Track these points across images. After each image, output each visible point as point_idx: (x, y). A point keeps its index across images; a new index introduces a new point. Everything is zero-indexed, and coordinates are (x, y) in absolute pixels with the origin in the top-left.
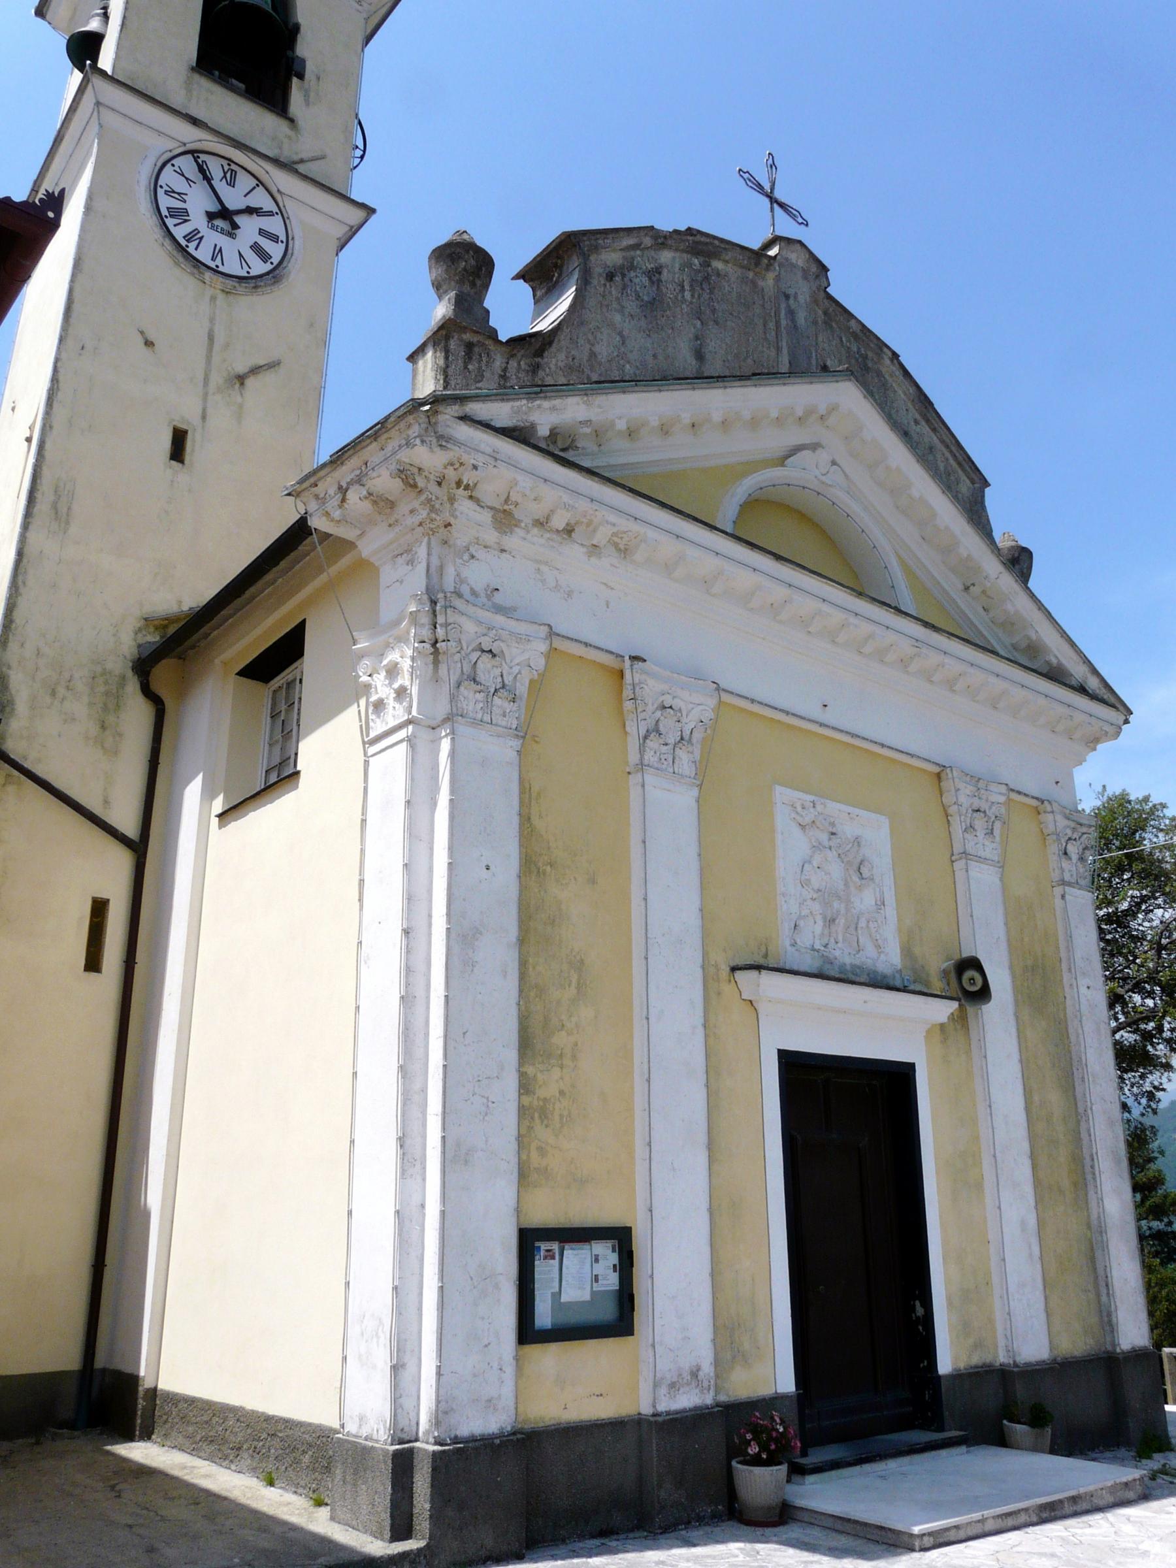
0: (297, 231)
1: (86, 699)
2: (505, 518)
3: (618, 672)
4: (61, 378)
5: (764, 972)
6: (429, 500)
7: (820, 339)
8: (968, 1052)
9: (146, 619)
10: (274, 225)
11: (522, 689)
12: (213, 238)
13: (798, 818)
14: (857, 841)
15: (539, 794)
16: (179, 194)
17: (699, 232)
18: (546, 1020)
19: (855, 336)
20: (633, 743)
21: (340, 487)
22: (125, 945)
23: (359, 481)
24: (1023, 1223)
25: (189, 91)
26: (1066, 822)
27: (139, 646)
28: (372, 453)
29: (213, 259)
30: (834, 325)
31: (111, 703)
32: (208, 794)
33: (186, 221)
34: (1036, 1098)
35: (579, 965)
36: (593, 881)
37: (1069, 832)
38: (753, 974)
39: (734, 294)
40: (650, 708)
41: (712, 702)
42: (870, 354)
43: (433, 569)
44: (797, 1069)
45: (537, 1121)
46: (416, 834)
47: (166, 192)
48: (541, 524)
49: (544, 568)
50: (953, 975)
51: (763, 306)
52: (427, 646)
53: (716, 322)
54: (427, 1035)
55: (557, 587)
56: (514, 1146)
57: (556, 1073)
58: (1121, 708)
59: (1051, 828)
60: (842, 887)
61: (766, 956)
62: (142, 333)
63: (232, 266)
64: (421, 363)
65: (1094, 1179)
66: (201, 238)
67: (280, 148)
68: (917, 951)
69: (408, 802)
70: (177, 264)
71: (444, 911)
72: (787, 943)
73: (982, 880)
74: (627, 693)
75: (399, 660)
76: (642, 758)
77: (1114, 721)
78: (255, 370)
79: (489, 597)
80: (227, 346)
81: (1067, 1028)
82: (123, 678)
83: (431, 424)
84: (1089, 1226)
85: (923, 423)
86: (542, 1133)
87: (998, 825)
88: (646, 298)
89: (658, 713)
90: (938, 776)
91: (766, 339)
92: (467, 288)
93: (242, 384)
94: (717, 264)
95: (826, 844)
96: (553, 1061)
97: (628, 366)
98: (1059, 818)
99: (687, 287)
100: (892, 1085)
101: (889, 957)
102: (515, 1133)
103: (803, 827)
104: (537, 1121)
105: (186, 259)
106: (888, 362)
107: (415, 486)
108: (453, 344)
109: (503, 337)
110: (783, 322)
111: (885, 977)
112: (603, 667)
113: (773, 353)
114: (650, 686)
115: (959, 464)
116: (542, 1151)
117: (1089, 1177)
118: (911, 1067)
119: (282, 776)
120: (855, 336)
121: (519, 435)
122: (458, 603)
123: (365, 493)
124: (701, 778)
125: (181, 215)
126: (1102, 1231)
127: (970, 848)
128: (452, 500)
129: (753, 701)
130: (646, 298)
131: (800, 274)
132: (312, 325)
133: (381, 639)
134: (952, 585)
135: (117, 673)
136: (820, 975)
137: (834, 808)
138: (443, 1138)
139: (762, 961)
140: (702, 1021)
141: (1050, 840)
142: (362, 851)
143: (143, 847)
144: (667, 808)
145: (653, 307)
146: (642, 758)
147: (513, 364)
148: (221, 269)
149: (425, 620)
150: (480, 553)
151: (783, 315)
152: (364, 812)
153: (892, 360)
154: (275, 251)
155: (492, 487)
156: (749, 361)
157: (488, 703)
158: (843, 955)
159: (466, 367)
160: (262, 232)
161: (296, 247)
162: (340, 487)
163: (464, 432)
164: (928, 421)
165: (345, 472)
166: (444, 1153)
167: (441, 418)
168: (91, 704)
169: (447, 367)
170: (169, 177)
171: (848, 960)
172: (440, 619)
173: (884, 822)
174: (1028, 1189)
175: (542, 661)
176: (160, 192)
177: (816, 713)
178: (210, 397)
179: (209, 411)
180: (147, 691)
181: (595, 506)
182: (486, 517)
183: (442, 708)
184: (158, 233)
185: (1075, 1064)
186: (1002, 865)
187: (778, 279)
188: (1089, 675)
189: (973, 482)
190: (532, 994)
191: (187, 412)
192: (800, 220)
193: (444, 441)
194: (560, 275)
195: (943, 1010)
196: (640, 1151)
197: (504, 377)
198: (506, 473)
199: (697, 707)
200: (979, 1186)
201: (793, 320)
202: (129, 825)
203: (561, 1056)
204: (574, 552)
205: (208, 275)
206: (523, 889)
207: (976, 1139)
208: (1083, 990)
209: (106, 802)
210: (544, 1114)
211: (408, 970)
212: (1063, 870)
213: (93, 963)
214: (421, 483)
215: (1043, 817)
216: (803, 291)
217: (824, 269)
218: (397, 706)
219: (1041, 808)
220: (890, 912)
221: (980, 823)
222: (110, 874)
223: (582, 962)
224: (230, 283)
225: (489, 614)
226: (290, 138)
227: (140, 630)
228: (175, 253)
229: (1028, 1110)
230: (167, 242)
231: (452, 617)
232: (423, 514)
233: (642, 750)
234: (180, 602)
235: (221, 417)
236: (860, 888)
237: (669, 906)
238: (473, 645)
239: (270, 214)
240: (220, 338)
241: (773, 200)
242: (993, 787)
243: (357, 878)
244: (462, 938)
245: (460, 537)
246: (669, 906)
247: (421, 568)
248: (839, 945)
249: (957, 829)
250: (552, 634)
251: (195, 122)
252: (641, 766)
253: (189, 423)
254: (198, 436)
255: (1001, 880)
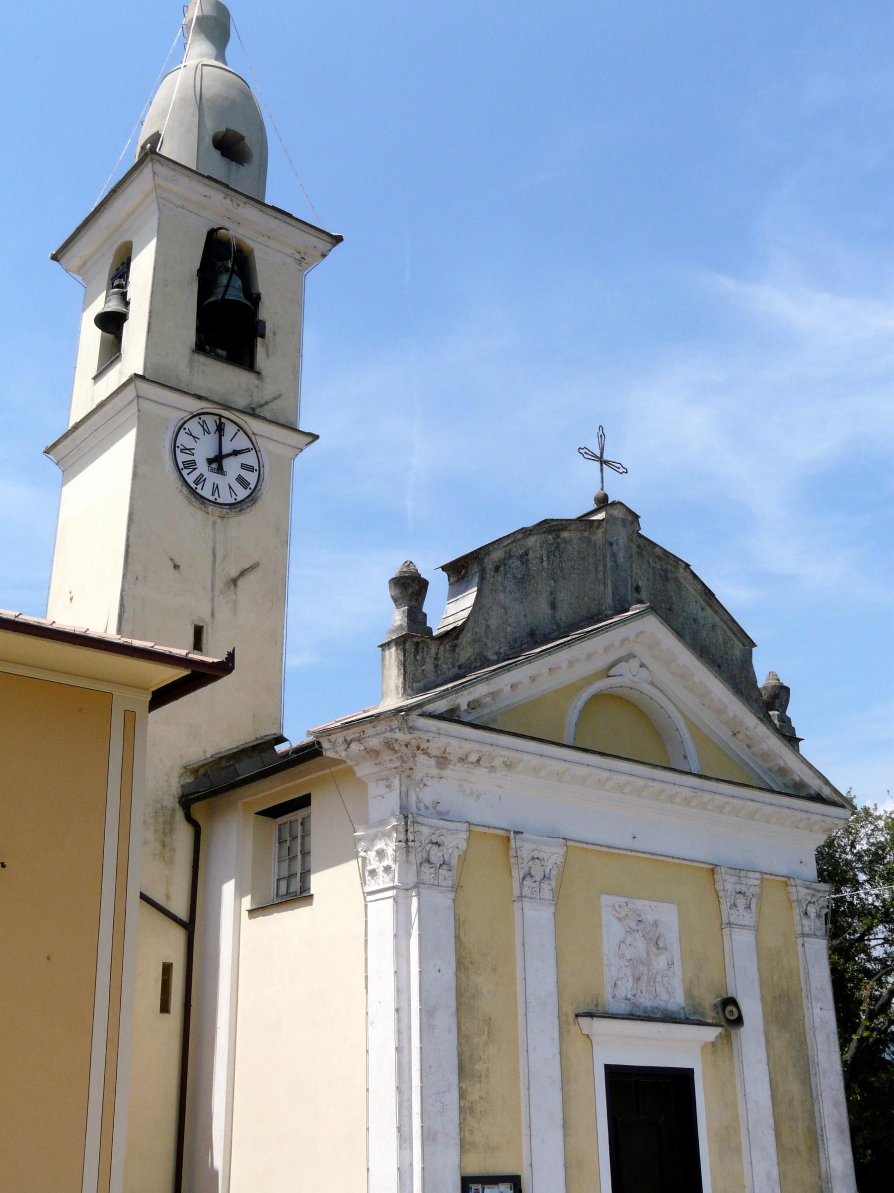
0: (266, 460)
1: (152, 828)
2: (443, 760)
3: (507, 838)
4: (125, 603)
5: (595, 1019)
6: (401, 757)
7: (634, 566)
8: (731, 1059)
9: (185, 767)
10: (250, 459)
11: (454, 862)
12: (212, 478)
13: (617, 915)
14: (656, 924)
15: (464, 922)
16: (189, 450)
17: (552, 520)
18: (472, 1055)
19: (659, 558)
20: (516, 884)
21: (346, 740)
22: (187, 995)
23: (359, 740)
24: (768, 1175)
25: (191, 368)
26: (807, 891)
27: (182, 786)
28: (369, 730)
29: (213, 495)
30: (644, 553)
31: (167, 830)
32: (240, 893)
33: (195, 469)
34: (781, 1088)
35: (488, 1021)
36: (494, 970)
37: (809, 898)
38: (589, 1019)
39: (576, 553)
40: (526, 860)
41: (562, 851)
42: (669, 567)
43: (403, 793)
44: (617, 1076)
45: (468, 1114)
46: (401, 954)
47: (182, 451)
48: (462, 760)
49: (464, 783)
50: (720, 1009)
51: (595, 555)
52: (403, 844)
53: (564, 578)
54: (410, 1068)
55: (472, 793)
56: (458, 1130)
57: (477, 1086)
58: (848, 806)
59: (794, 898)
60: (645, 956)
61: (597, 1005)
62: (172, 560)
63: (225, 497)
64: (387, 652)
65: (823, 1144)
66: (205, 480)
67: (252, 396)
68: (696, 993)
69: (395, 935)
70: (190, 503)
71: (418, 998)
72: (610, 997)
73: (742, 944)
74: (512, 853)
75: (385, 847)
76: (521, 893)
77: (844, 816)
78: (243, 573)
79: (434, 808)
80: (224, 559)
81: (805, 1037)
82: (173, 810)
83: (405, 719)
84: (820, 1177)
85: (708, 608)
86: (471, 1122)
87: (754, 901)
88: (519, 576)
89: (531, 863)
90: (713, 870)
91: (597, 579)
92: (414, 603)
93: (235, 585)
94: (565, 535)
95: (635, 928)
96: (476, 1079)
97: (509, 628)
98: (800, 889)
99: (545, 559)
100: (682, 1079)
101: (677, 1000)
102: (458, 1122)
103: (620, 919)
104: (468, 1114)
105: (196, 498)
106: (682, 570)
107: (394, 749)
108: (408, 646)
109: (435, 633)
110: (609, 565)
111: (673, 1012)
112: (497, 836)
113: (602, 587)
114: (525, 847)
115: (734, 633)
116: (471, 1132)
117: (820, 1142)
118: (691, 1071)
119: (295, 894)
120: (659, 558)
121: (451, 716)
122: (420, 819)
123: (362, 748)
124: (557, 900)
125: (191, 465)
126: (828, 1180)
127: (732, 920)
128: (414, 756)
129: (587, 843)
130: (519, 576)
131: (620, 523)
132: (278, 530)
133: (373, 831)
134: (725, 734)
135: (169, 807)
136: (631, 1016)
137: (639, 904)
138: (422, 1127)
139: (593, 1009)
140: (559, 1050)
141: (795, 904)
142: (366, 959)
143: (192, 925)
144: (537, 919)
145: (523, 581)
146: (521, 893)
147: (442, 648)
148: (219, 501)
149: (402, 829)
150: (429, 782)
151: (608, 559)
152: (366, 935)
153: (685, 569)
154: (251, 478)
155: (435, 747)
156: (586, 599)
157: (437, 874)
158: (646, 1001)
159: (415, 659)
160: (244, 466)
161: (266, 473)
162: (346, 740)
163: (423, 722)
164: (711, 606)
165: (350, 734)
166: (422, 1135)
167: (410, 717)
168: (156, 831)
169: (405, 661)
170: (184, 440)
171: (649, 1004)
172: (410, 829)
173: (674, 909)
174: (773, 1151)
175: (465, 844)
176: (178, 451)
177: (628, 843)
178: (216, 599)
179: (216, 610)
180: (189, 819)
181: (494, 748)
182: (433, 762)
183: (412, 879)
184: (178, 483)
185: (811, 1062)
186: (756, 928)
187: (605, 533)
188: (823, 786)
189: (744, 645)
190: (464, 1041)
191: (202, 613)
192: (622, 470)
193: (411, 729)
194: (466, 573)
195: (711, 1034)
196: (525, 1131)
197: (437, 659)
198: (444, 740)
199: (553, 854)
200: (738, 1150)
201: (615, 561)
202: (182, 912)
203: (480, 1076)
204: (481, 772)
205: (210, 508)
206: (458, 979)
207: (736, 1117)
208: (817, 1011)
209: (168, 897)
210: (472, 1111)
211: (399, 1032)
212: (803, 926)
213: (165, 1008)
214: (397, 747)
215: (789, 888)
216: (621, 536)
217: (637, 517)
218: (385, 875)
219: (788, 882)
220: (677, 968)
221: (741, 902)
222: (170, 945)
223: (490, 1019)
224: (225, 510)
225: (435, 821)
226: (257, 386)
227: (182, 775)
228: (189, 495)
229: (773, 1097)
230: (184, 490)
231: (417, 828)
232: (398, 764)
233: (521, 887)
234: (205, 752)
235: (224, 613)
236: (657, 955)
237: (539, 980)
238: (428, 840)
239: (247, 450)
240: (220, 554)
241: (603, 462)
242: (751, 874)
243: (364, 975)
244: (427, 1013)
245: (418, 774)
246: (539, 980)
247: (396, 793)
248: (644, 994)
249: (724, 907)
250: (470, 824)
251: (199, 397)
252: (521, 897)
253: (204, 621)
254: (210, 629)
255: (756, 939)
